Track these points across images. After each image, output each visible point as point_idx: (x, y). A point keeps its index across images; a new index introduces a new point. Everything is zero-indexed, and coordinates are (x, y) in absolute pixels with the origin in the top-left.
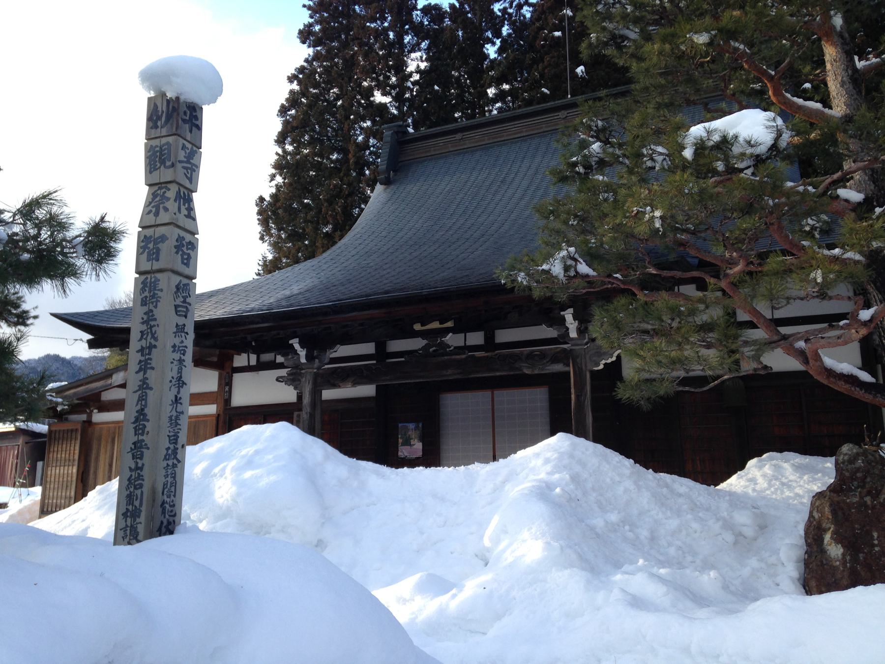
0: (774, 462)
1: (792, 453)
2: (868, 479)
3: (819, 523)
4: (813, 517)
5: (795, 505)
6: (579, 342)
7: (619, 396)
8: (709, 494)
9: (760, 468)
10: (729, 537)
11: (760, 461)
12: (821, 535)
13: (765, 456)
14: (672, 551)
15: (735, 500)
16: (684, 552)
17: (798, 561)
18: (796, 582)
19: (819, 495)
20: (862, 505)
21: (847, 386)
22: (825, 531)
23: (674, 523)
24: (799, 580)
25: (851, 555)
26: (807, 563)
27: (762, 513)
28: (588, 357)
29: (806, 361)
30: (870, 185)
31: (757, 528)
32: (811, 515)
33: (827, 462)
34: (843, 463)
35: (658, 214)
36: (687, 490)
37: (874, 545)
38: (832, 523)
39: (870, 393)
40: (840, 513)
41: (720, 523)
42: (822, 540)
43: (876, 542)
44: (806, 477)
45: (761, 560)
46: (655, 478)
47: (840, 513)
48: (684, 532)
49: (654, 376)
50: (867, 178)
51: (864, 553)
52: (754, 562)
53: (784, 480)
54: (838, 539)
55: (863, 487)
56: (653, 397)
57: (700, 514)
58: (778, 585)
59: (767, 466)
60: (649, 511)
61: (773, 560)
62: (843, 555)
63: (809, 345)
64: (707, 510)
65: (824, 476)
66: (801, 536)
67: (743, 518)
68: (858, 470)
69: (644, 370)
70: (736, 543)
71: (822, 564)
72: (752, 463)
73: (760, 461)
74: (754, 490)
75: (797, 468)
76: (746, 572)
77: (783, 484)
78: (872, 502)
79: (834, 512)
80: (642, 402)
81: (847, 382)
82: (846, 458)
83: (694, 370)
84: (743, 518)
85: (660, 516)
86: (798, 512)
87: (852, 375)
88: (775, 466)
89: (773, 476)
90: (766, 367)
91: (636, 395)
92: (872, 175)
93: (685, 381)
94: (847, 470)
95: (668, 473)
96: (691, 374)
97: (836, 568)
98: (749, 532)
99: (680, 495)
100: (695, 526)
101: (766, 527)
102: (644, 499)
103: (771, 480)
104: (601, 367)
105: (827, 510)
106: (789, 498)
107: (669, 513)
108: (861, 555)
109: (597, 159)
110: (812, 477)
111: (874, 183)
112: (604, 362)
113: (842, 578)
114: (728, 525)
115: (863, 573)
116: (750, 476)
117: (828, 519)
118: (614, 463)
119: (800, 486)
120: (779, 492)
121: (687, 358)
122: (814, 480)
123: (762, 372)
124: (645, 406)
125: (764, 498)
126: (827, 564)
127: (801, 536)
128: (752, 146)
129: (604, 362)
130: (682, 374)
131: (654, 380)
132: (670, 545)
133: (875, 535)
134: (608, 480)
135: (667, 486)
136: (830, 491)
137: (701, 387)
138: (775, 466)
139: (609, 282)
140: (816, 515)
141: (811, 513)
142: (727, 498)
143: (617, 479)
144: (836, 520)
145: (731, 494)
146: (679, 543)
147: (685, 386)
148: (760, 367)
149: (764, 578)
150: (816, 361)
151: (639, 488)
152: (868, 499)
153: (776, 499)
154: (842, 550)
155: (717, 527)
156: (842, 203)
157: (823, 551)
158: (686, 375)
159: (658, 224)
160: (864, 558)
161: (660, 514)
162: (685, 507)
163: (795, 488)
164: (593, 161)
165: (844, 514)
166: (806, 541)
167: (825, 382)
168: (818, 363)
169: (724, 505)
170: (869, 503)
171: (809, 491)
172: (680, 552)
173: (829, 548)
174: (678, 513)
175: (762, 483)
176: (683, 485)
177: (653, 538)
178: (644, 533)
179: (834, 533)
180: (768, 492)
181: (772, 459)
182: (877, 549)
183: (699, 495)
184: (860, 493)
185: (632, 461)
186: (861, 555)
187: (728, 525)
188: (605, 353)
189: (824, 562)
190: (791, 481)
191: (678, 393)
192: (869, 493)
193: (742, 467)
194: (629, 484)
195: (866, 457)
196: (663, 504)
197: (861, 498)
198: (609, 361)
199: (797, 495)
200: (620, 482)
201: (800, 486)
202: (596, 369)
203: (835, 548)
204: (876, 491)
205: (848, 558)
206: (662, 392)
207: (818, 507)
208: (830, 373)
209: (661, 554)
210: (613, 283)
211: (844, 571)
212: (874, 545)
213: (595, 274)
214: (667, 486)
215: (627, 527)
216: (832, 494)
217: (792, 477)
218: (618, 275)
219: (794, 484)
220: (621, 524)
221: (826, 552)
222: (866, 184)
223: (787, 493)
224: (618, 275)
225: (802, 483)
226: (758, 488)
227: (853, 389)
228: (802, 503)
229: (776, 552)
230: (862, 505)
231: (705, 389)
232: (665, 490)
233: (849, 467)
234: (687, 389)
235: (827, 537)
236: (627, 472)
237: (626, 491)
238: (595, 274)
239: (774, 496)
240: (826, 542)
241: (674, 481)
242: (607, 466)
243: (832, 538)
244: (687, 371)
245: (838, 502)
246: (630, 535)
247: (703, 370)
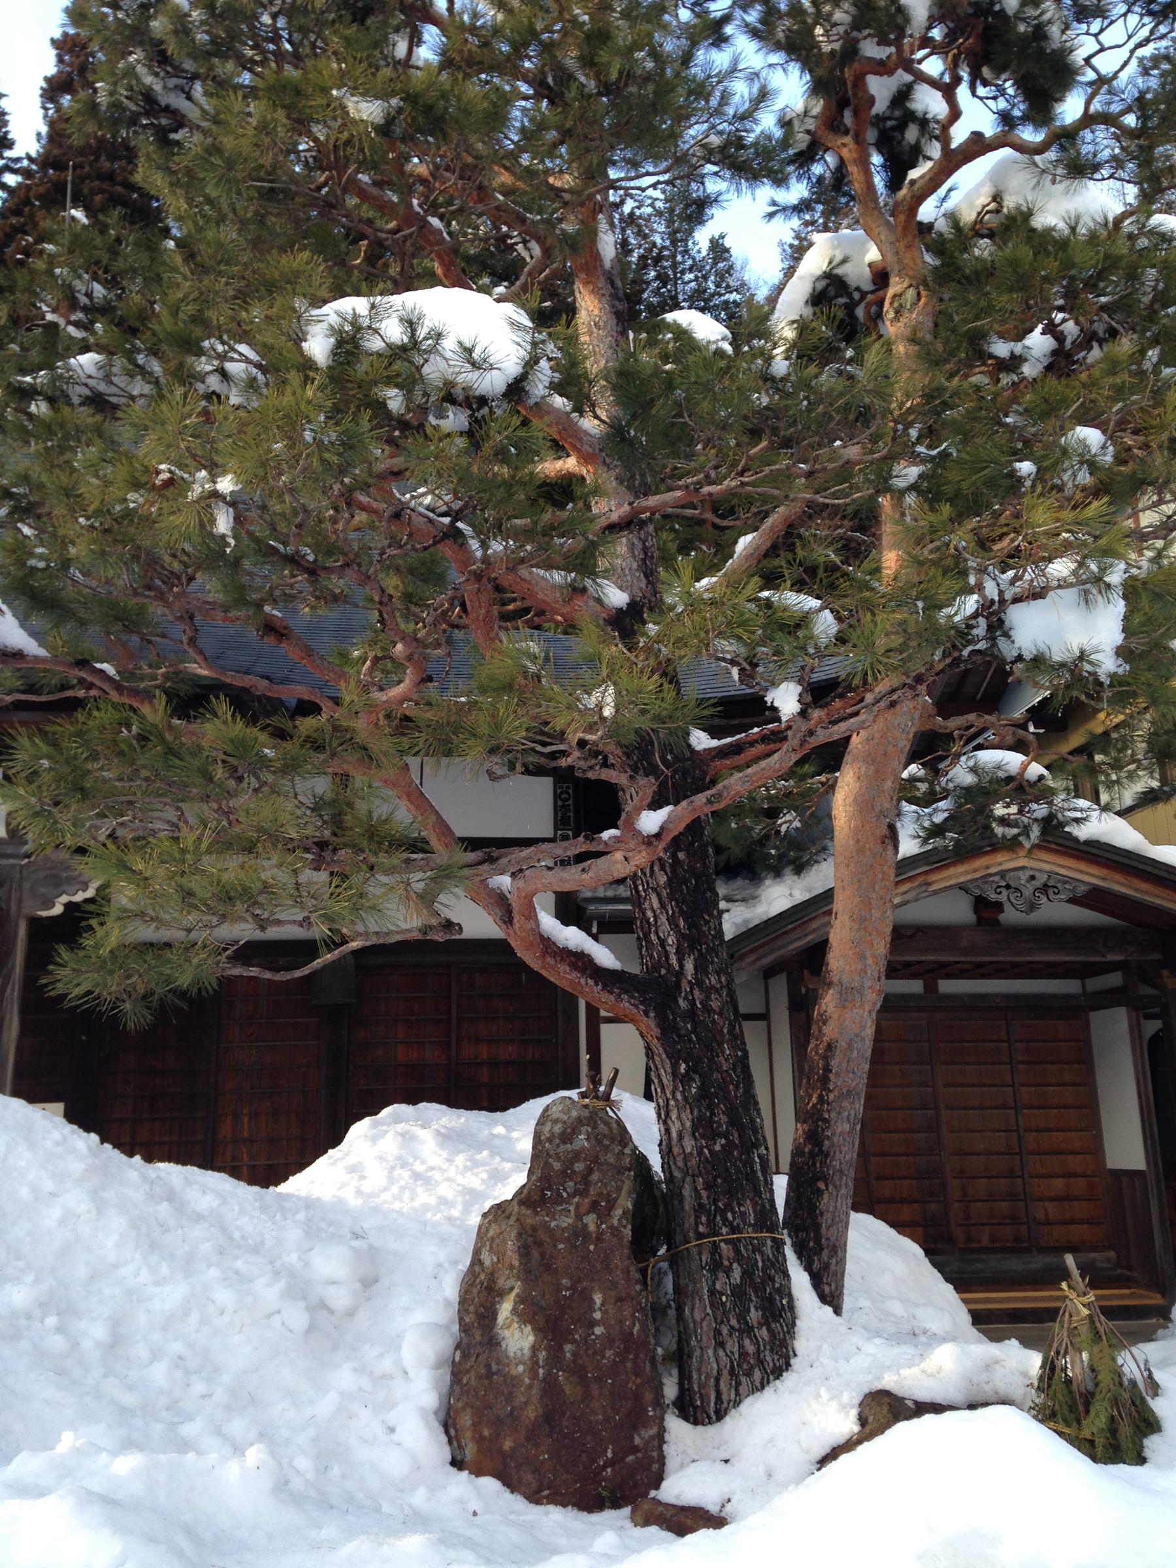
0: (401, 1127)
1: (434, 1106)
2: (595, 1176)
3: (492, 1277)
4: (481, 1263)
5: (436, 1225)
6: (10, 850)
7: (60, 988)
8: (264, 1209)
9: (374, 1139)
10: (297, 1317)
11: (374, 1125)
12: (494, 1304)
13: (385, 1112)
14: (159, 1374)
15: (321, 1221)
16: (187, 1372)
17: (437, 1366)
18: (432, 1418)
19: (499, 1211)
20: (580, 1232)
21: (575, 975)
22: (502, 1294)
23: (172, 1295)
24: (436, 1413)
25: (548, 1349)
26: (457, 1373)
27: (371, 1247)
28: (27, 885)
29: (507, 918)
30: (639, 580)
31: (358, 1286)
32: (476, 1260)
33: (496, 1123)
34: (550, 1140)
35: (226, 485)
36: (215, 1204)
37: (592, 1324)
38: (519, 1279)
39: (611, 992)
40: (535, 1254)
41: (282, 1284)
42: (494, 1314)
43: (597, 1315)
44: (460, 1159)
45: (361, 1370)
46: (143, 1177)
47: (535, 1254)
48: (195, 1317)
49: (166, 935)
50: (635, 565)
51: (574, 1341)
52: (344, 1377)
53: (419, 1167)
54: (528, 1313)
55: (583, 1193)
56: (160, 990)
57: (239, 1264)
58: (392, 1430)
59: (390, 1136)
60: (116, 1266)
61: (387, 1365)
62: (534, 1349)
63: (521, 883)
64: (256, 1250)
65: (493, 1154)
66: (447, 1302)
67: (331, 1266)
68: (577, 1155)
69: (141, 915)
70: (311, 1329)
71: (490, 1374)
72: (359, 1130)
73: (374, 1125)
74: (359, 1192)
75: (447, 1138)
76: (327, 1404)
77: (416, 1176)
78: (598, 1227)
79: (524, 1252)
80: (127, 1006)
81: (574, 967)
82: (558, 1129)
83: (278, 922)
84: (331, 1266)
85: (145, 1276)
86: (443, 1240)
87: (582, 953)
88: (403, 1135)
89: (399, 1158)
90: (448, 925)
91: (112, 986)
92: (644, 560)
93: (248, 952)
94: (558, 1158)
95: (177, 1162)
96: (273, 933)
97: (514, 1381)
98: (340, 1298)
99: (198, 1218)
100: (224, 1296)
101: (376, 1281)
102: (110, 1238)
103: (393, 1168)
104: (58, 910)
105: (511, 1245)
106: (426, 1208)
107: (165, 1270)
108: (568, 1348)
109: (87, 392)
110: (471, 1159)
111: (646, 576)
112: (64, 899)
113: (526, 1403)
114: (299, 1288)
115: (567, 1389)
116: (352, 1160)
117: (511, 1267)
118: (49, 1144)
119: (448, 1179)
120: (407, 1193)
121: (266, 887)
122: (476, 1164)
123: (440, 937)
124: (134, 1016)
125: (376, 1210)
126: (498, 1372)
127: (447, 1302)
128: (475, 365)
129: (64, 899)
130: (244, 931)
131: (168, 945)
132: (156, 1354)
133: (598, 1298)
134: (24, 1192)
135: (171, 1196)
136: (521, 1203)
137: (277, 970)
138: (403, 1135)
139: (81, 681)
140: (487, 1259)
141: (477, 1252)
142: (301, 1216)
143: (49, 1185)
144: (528, 1274)
145: (310, 1204)
146: (178, 1347)
147: (247, 963)
148: (434, 922)
149: (364, 1415)
150: (528, 918)
151: (100, 1206)
152: (590, 1220)
153: (400, 1213)
154: (531, 1338)
155: (269, 1292)
156: (592, 603)
157: (492, 1342)
158: (258, 935)
159: (223, 523)
160: (574, 1354)
161: (144, 1272)
162: (206, 1247)
163: (438, 1183)
164: (77, 393)
165: (543, 1255)
166: (461, 1319)
167: (535, 966)
168: (532, 924)
169: (294, 1235)
170: (592, 1227)
171: (472, 1195)
172: (179, 1374)
173: (506, 1333)
174: (188, 1265)
175: (376, 1178)
176: (208, 1190)
177: (116, 1343)
178: (94, 1332)
179: (521, 1299)
180: (386, 1196)
181: (397, 1120)
182: (598, 1331)
183: (243, 1212)
184: (578, 1206)
185: (94, 1137)
186: (568, 1348)
187: (299, 1288)
188: (70, 880)
189: (494, 1368)
190: (432, 1168)
191: (227, 983)
192: (594, 1207)
193: (335, 1139)
194: (76, 1199)
195: (594, 1128)
196: (153, 1246)
197: (579, 1217)
198: (79, 897)
199: (443, 1201)
200: (53, 1195)
201: (448, 1179)
202: (44, 914)
203: (517, 1334)
204: (608, 1202)
205: (542, 1355)
206: (184, 980)
207: (493, 1239)
208: (547, 945)
209: (130, 1388)
210: (91, 686)
211: (530, 1386)
212: (592, 1324)
213: (42, 652)
214: (171, 1196)
215: (51, 1321)
216: (524, 1210)
217: (433, 1161)
218: (105, 666)
219: (437, 1175)
220: (37, 1313)
221: (499, 1344)
222: (633, 576)
223: (424, 1197)
224: (105, 666)
225: (452, 1172)
226: (367, 1187)
227: (583, 981)
228: (450, 1219)
229: (393, 1344)
230: (580, 1232)
231: (298, 973)
232: (164, 1208)
233: (562, 1148)
234: (254, 971)
235: (505, 1309)
236: (77, 1167)
237: (67, 1218)
238: (42, 652)
239: (397, 1206)
240: (501, 1319)
241: (188, 1182)
242: (28, 1155)
243: (514, 1311)
244: (263, 925)
245: (534, 1229)
246: (57, 1342)
247: (306, 922)
